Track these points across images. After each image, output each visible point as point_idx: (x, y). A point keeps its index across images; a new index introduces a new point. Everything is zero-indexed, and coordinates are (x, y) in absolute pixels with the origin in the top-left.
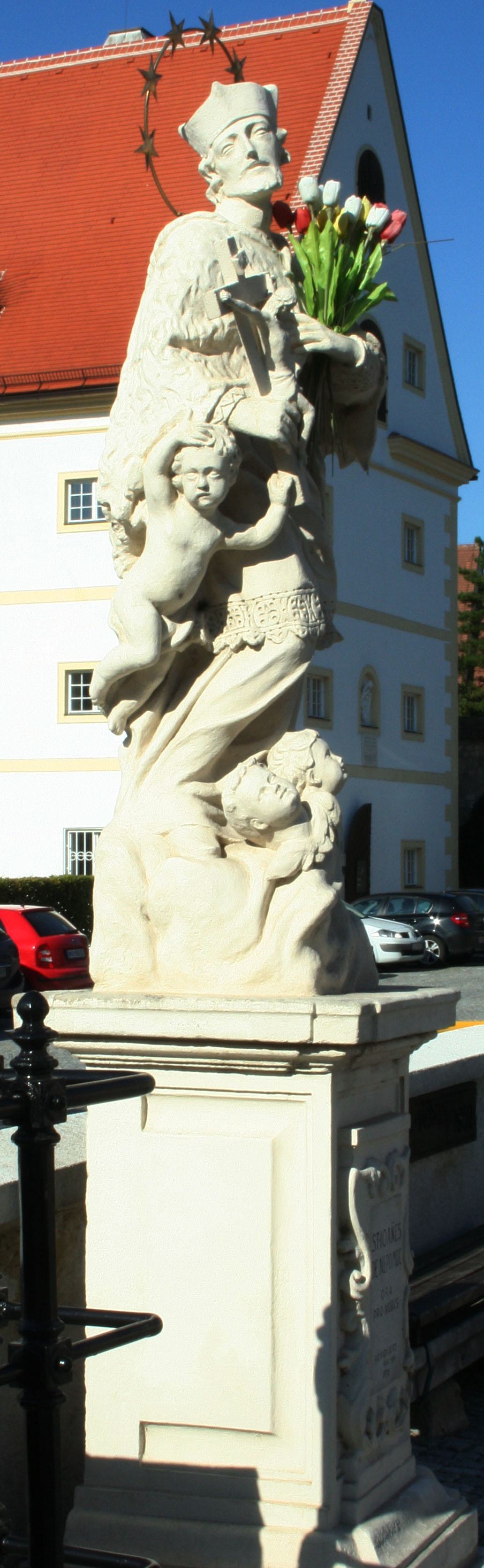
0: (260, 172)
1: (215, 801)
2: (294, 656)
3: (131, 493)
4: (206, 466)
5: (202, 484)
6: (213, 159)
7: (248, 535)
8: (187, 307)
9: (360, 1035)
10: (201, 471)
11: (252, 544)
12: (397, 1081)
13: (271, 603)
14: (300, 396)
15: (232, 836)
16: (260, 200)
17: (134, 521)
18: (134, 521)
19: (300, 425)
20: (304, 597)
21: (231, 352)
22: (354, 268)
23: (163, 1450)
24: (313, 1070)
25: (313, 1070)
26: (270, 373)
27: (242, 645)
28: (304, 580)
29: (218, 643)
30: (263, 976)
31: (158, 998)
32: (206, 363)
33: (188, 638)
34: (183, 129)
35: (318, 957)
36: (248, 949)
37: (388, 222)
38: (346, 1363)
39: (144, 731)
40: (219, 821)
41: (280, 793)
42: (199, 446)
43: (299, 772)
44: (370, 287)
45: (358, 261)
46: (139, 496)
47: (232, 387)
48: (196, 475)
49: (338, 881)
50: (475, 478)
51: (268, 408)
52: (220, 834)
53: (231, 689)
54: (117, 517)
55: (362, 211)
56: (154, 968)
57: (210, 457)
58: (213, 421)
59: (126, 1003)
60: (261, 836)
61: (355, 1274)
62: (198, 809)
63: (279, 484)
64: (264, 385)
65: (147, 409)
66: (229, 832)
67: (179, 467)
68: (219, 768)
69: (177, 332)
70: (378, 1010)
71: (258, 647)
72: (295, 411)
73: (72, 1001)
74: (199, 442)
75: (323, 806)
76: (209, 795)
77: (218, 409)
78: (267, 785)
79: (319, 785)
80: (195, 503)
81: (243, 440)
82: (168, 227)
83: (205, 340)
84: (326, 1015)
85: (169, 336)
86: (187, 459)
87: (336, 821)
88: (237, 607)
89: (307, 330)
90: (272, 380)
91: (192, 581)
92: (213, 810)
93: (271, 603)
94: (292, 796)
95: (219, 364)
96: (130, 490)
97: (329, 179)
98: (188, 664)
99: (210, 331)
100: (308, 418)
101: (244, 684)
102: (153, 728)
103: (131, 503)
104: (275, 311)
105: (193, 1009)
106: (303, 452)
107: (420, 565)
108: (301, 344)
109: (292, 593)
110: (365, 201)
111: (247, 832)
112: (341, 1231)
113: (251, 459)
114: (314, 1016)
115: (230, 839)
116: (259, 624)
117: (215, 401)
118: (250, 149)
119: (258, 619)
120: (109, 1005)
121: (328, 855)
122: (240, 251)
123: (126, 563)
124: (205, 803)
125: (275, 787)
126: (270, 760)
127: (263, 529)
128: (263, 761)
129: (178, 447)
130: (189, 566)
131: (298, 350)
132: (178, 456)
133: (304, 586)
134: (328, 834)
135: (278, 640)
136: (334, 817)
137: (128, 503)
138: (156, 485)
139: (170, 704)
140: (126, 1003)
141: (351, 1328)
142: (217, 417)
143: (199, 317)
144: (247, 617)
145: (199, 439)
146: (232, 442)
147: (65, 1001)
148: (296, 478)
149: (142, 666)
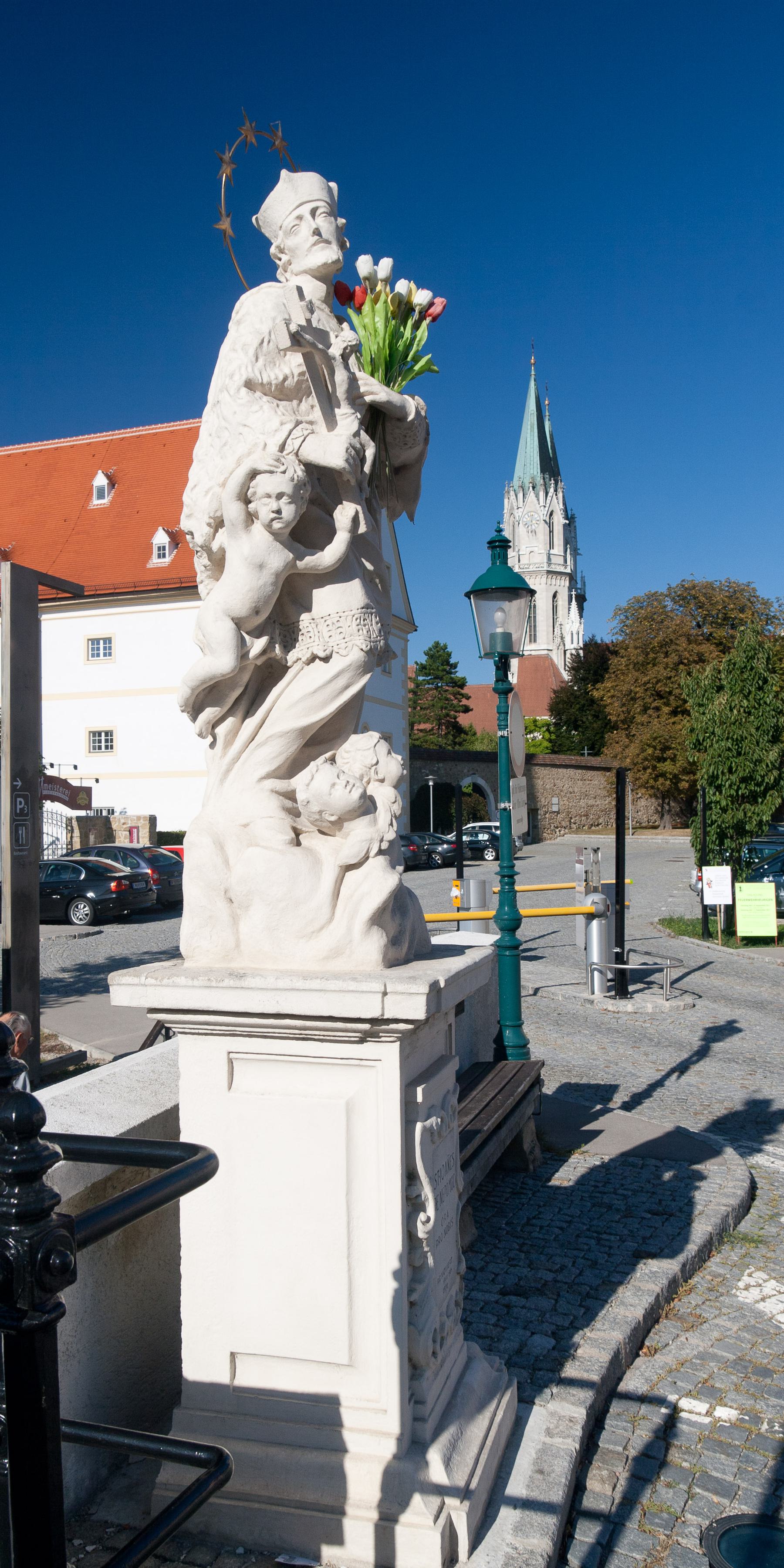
0: (323, 249)
1: (290, 796)
2: (359, 667)
3: (212, 521)
4: (279, 491)
5: (275, 508)
6: (283, 241)
7: (317, 559)
8: (260, 356)
9: (428, 1011)
10: (274, 496)
11: (320, 568)
12: (447, 1028)
13: (338, 616)
14: (363, 433)
15: (305, 826)
16: (321, 275)
17: (215, 546)
18: (215, 546)
19: (363, 460)
20: (366, 615)
21: (301, 401)
22: (405, 339)
23: (250, 1377)
24: (383, 1039)
25: (383, 1039)
26: (337, 410)
27: (313, 658)
28: (367, 601)
29: (291, 657)
30: (336, 953)
31: (241, 976)
32: (278, 406)
33: (264, 652)
34: (257, 218)
35: (384, 934)
36: (322, 928)
37: (431, 304)
38: (415, 1297)
39: (226, 736)
40: (295, 813)
41: (349, 788)
42: (271, 472)
43: (365, 769)
44: (416, 360)
45: (408, 333)
46: (218, 524)
47: (301, 422)
48: (269, 500)
49: (400, 865)
50: (416, 630)
51: (334, 443)
52: (294, 825)
53: (304, 696)
54: (200, 544)
55: (410, 292)
56: (238, 946)
57: (281, 483)
58: (285, 452)
59: (211, 977)
60: (331, 827)
61: (422, 1216)
62: (273, 806)
63: (345, 513)
64: (331, 421)
65: (225, 444)
66: (303, 823)
67: (255, 493)
68: (294, 766)
69: (251, 376)
70: (442, 984)
71: (326, 659)
72: (358, 446)
73: (162, 979)
74: (272, 469)
75: (388, 801)
76: (285, 790)
77: (289, 441)
78: (337, 780)
79: (382, 781)
80: (268, 527)
81: (311, 468)
82: (243, 297)
83: (277, 385)
84: (396, 993)
85: (244, 378)
86: (262, 484)
87: (398, 813)
88: (308, 624)
89: (366, 384)
90: (338, 417)
91: (267, 599)
92: (289, 804)
93: (338, 616)
94: (360, 791)
95: (289, 409)
96: (210, 517)
97: (382, 258)
98: (265, 677)
99: (281, 378)
100: (370, 452)
101: (315, 692)
102: (234, 733)
103: (212, 530)
104: (341, 352)
105: (273, 987)
106: (366, 485)
107: (390, 673)
108: (361, 396)
109: (357, 612)
110: (413, 285)
111: (319, 823)
112: (410, 1177)
113: (320, 488)
114: (385, 994)
115: (304, 829)
116: (327, 639)
117: (286, 433)
118: (315, 226)
119: (326, 635)
120: (196, 983)
121: (391, 842)
122: (307, 299)
123: (209, 587)
124: (281, 797)
125: (344, 783)
126: (337, 759)
127: (332, 553)
128: (333, 760)
129: (253, 474)
130: (265, 585)
131: (358, 401)
132: (253, 484)
133: (366, 607)
134: (391, 824)
135: (344, 652)
136: (397, 809)
137: (207, 530)
138: (233, 511)
139: (249, 712)
140: (211, 977)
141: (417, 1264)
142: (288, 448)
143: (272, 365)
144: (316, 633)
145: (271, 466)
146: (302, 470)
147: (156, 979)
148: (359, 508)
149: (223, 676)
